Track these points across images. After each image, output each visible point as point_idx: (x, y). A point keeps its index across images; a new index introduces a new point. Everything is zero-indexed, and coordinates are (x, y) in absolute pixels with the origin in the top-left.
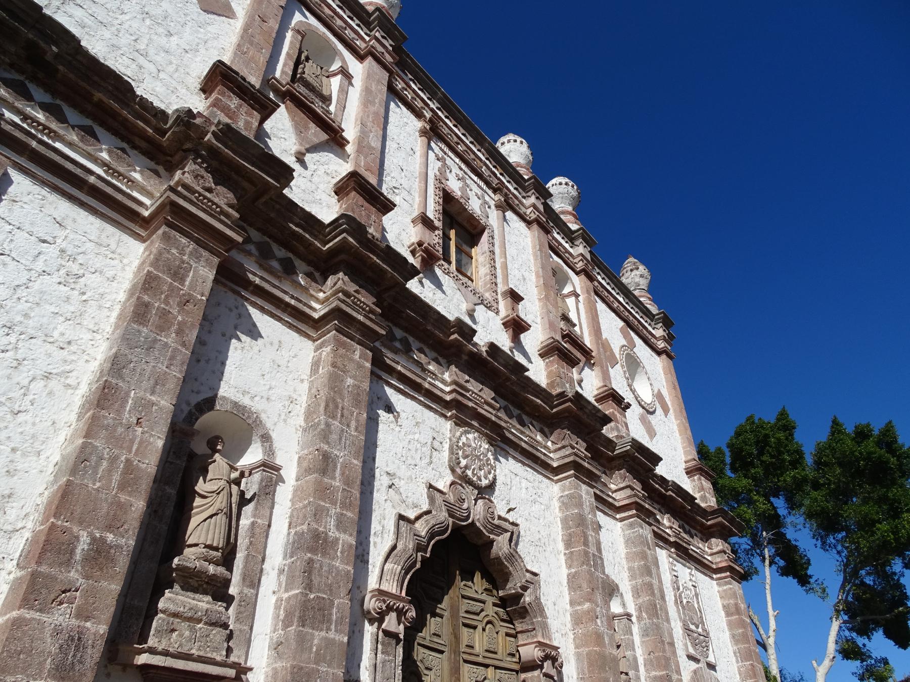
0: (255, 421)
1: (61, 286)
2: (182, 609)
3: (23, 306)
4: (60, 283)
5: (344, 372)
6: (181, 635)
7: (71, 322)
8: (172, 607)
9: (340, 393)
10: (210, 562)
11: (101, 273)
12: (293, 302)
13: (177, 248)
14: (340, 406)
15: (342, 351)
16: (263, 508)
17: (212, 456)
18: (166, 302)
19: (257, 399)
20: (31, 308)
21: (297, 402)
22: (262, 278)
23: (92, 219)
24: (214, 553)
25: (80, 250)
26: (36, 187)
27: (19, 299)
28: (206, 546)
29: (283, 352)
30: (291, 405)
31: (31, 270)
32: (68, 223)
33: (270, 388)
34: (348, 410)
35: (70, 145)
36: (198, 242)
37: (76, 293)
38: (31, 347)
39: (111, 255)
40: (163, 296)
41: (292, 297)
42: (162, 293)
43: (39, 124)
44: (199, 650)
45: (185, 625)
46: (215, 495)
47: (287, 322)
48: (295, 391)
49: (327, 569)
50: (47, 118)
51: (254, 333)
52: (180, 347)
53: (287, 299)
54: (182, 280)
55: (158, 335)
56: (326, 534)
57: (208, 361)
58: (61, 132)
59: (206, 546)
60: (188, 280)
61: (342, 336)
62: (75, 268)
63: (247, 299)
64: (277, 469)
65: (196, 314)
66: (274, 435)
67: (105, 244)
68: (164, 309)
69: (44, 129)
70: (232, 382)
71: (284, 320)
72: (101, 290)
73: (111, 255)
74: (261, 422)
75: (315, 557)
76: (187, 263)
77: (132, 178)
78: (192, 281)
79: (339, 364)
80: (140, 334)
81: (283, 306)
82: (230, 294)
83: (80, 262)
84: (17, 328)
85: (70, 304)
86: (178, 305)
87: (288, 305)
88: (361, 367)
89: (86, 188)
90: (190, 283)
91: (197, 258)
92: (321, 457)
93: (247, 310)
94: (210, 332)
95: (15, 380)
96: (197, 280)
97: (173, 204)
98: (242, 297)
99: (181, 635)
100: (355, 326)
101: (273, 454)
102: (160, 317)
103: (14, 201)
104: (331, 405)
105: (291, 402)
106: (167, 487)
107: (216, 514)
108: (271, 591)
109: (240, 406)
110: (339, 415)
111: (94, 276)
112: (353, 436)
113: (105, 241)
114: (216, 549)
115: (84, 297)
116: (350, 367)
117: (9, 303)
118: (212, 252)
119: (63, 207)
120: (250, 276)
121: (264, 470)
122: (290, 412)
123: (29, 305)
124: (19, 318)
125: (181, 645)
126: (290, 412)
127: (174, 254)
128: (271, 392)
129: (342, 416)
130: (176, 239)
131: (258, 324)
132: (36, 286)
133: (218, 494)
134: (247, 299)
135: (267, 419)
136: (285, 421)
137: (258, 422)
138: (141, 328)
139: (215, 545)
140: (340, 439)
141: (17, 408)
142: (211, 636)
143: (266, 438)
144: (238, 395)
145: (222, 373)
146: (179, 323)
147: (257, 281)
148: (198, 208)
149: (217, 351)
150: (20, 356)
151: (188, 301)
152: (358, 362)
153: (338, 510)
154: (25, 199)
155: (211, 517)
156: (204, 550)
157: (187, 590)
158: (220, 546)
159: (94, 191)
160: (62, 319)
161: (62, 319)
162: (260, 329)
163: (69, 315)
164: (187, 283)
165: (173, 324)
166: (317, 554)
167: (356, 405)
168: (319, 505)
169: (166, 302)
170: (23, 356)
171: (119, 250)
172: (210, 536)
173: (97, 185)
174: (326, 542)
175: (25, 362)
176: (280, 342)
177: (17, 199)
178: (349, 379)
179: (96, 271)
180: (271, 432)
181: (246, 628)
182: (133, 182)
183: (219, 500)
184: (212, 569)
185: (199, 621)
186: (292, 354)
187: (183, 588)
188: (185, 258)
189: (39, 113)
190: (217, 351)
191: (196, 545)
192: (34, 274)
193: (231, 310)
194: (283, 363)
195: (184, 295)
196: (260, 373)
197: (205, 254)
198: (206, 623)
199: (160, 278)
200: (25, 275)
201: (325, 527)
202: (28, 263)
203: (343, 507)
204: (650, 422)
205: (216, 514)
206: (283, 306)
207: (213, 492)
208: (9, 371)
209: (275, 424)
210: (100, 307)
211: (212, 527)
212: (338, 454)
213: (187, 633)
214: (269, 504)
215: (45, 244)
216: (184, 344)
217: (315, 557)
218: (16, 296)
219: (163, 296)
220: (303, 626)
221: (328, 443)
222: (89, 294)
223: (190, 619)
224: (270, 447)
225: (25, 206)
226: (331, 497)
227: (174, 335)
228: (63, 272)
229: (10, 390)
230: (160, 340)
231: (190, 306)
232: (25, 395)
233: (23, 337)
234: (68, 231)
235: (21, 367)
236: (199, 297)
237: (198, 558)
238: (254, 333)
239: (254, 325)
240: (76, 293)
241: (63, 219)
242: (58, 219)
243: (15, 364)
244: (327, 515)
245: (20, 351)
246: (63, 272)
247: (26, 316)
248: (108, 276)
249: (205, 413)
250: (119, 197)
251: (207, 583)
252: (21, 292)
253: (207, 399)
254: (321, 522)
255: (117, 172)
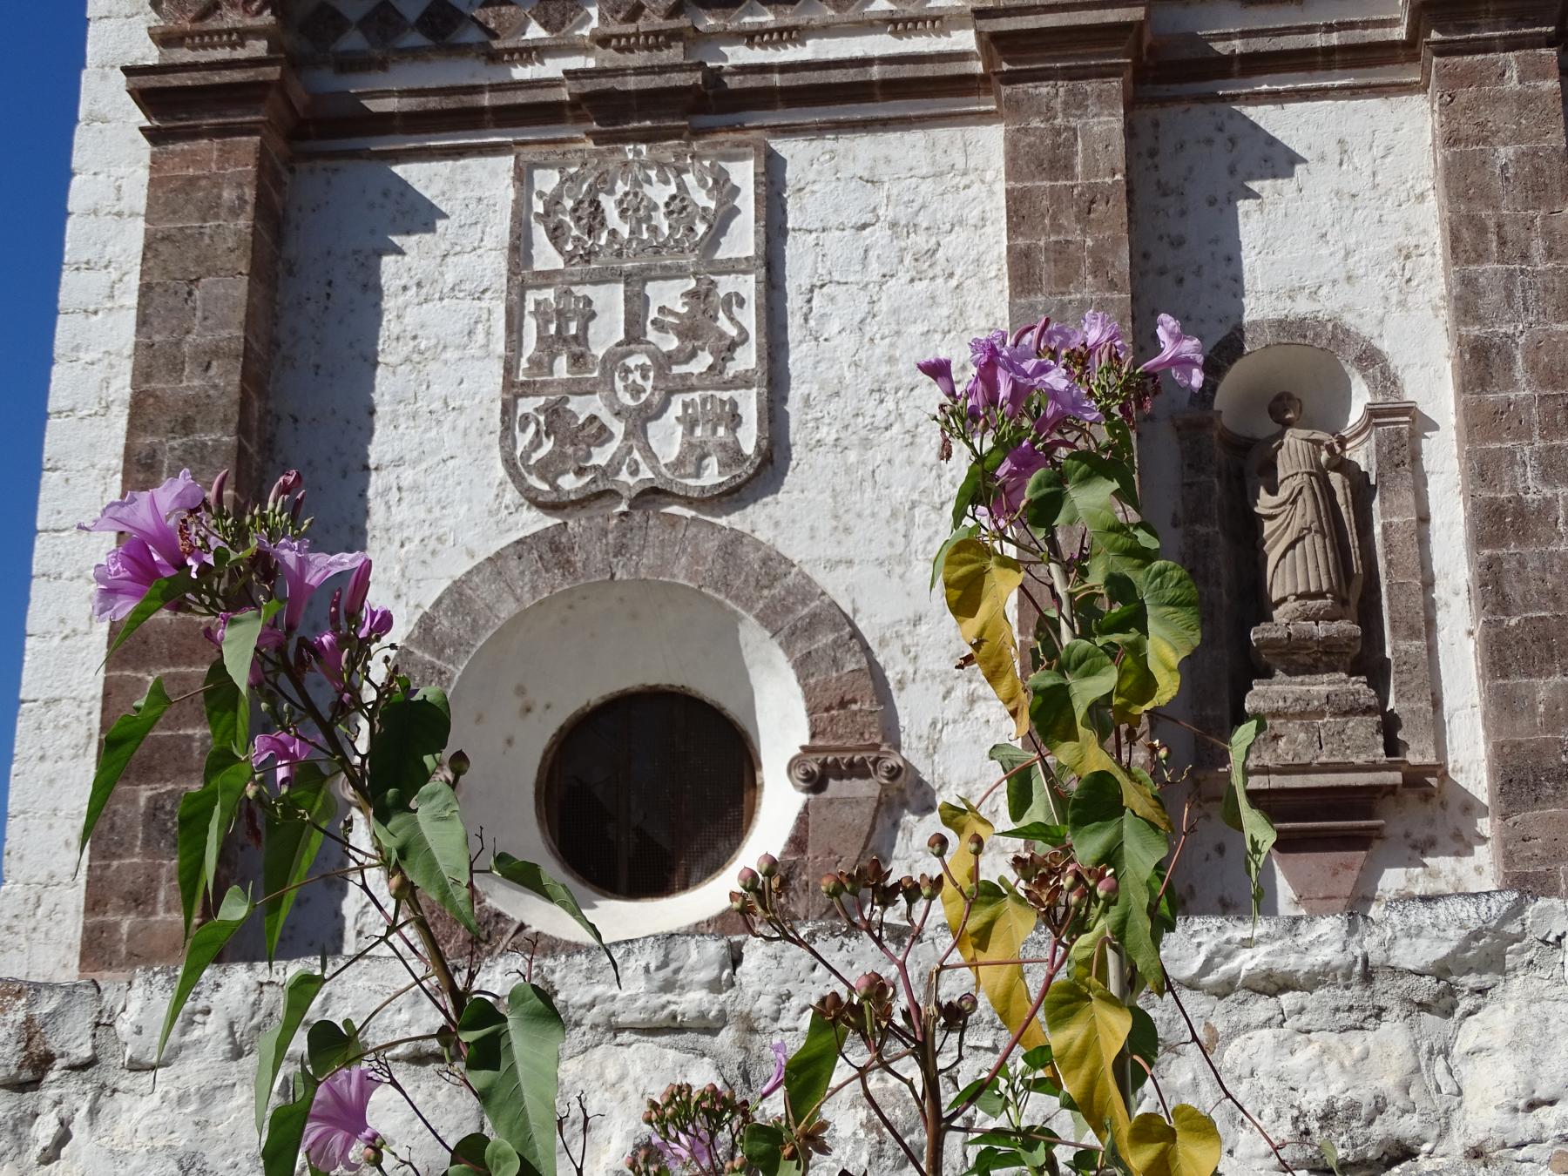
0: (1334, 336)
1: (917, 283)
2: (1281, 704)
3: (882, 347)
4: (912, 281)
5: (1485, 140)
6: (1293, 741)
7: (953, 334)
8: (1263, 706)
9: (1486, 196)
10: (1316, 619)
11: (961, 222)
12: (1335, 39)
13: (1039, 113)
14: (1491, 224)
15: (1465, 94)
16: (1398, 493)
17: (1281, 435)
18: (1057, 228)
19: (1324, 291)
20: (892, 345)
21: (1421, 251)
22: (1245, 34)
23: (916, 137)
24: (1319, 603)
25: (916, 206)
26: (815, 143)
27: (872, 340)
28: (1299, 597)
29: (1356, 160)
30: (1409, 265)
31: (866, 285)
32: (883, 171)
33: (1347, 254)
34: (1515, 222)
35: (827, 30)
36: (1070, 75)
37: (940, 281)
38: (918, 403)
39: (965, 181)
40: (1047, 221)
41: (1329, 28)
42: (1043, 216)
43: (770, 32)
44: (1331, 754)
45: (1295, 725)
46: (1288, 507)
47: (1341, 88)
48: (1408, 229)
49: (1537, 564)
50: (776, 13)
51: (1281, 161)
52: (1107, 295)
53: (1319, 40)
54: (1068, 169)
55: (1063, 294)
56: (1519, 500)
57: (1198, 272)
58: (802, 20)
59: (1299, 597)
60: (1079, 160)
61: (1456, 59)
62: (920, 241)
63: (1234, 98)
64: (1409, 410)
65: (1114, 213)
66: (1385, 346)
67: (946, 168)
68: (1056, 242)
69: (781, 35)
70: (1260, 287)
71: (1333, 89)
72: (973, 254)
73: (965, 181)
74: (1347, 332)
75: (1502, 552)
76: (1067, 129)
77: (935, 13)
78: (1085, 157)
79: (1468, 129)
80: (1036, 310)
81: (1320, 59)
82: (1199, 110)
83: (925, 225)
84: (888, 386)
85: (939, 305)
86: (1078, 220)
87: (1329, 51)
88: (1530, 101)
89: (877, 91)
90: (1084, 165)
91: (1078, 108)
92: (1467, 356)
93: (1245, 118)
94: (1183, 213)
95: (919, 461)
96: (1094, 151)
97: (996, 37)
98: (1223, 98)
99: (1293, 741)
100: (1487, 12)
101: (1394, 383)
102: (1055, 261)
103: (800, 190)
104: (1466, 235)
105: (1407, 257)
106: (1197, 527)
107: (1300, 539)
108: (1462, 633)
109: (1292, 323)
110: (1494, 246)
111: (953, 235)
112: (1542, 274)
113: (944, 162)
114: (1320, 595)
115: (953, 282)
116: (1499, 118)
117: (863, 354)
118: (1103, 73)
119: (863, 149)
120: (1220, 47)
121: (1377, 425)
122: (1409, 280)
123: (887, 341)
124: (884, 369)
125: (1296, 755)
126: (1409, 280)
127: (1036, 128)
128: (1351, 261)
129: (1503, 242)
130: (1030, 97)
131: (1278, 135)
132: (883, 306)
133: (1294, 502)
134: (1234, 98)
135: (1359, 321)
136: (1402, 304)
137: (1340, 335)
138: (1032, 298)
139: (1313, 589)
140: (1510, 296)
141: (937, 500)
142: (1349, 732)
143: (1370, 358)
144: (1280, 306)
145: (1238, 279)
146: (1092, 252)
147: (1238, 46)
148: (1038, 13)
149: (1211, 242)
150: (909, 425)
151: (1092, 202)
152: (1519, 94)
153: (1539, 444)
154: (811, 176)
155: (1292, 546)
156: (1297, 604)
157: (1297, 674)
158: (1325, 587)
159: (893, 89)
160: (938, 337)
161: (938, 337)
162: (1285, 142)
163: (945, 325)
164: (1079, 169)
165: (1081, 260)
166: (1506, 545)
167: (1536, 198)
168: (1488, 451)
169: (1057, 228)
170: (914, 422)
171: (971, 165)
172: (1300, 578)
173: (888, 76)
174: (1524, 516)
175: (921, 429)
176: (1340, 142)
177: (802, 184)
178: (1502, 150)
179: (953, 225)
180: (1376, 343)
181: (1425, 705)
182: (940, 18)
183: (1299, 511)
184: (1321, 630)
185: (1322, 714)
186: (1377, 151)
187: (1288, 673)
188: (1058, 121)
189: (764, 14)
190: (1211, 242)
191: (1284, 600)
192: (873, 289)
193: (1209, 142)
194: (1361, 183)
195: (1081, 195)
196: (1314, 236)
197: (1090, 86)
198: (1334, 715)
199: (1029, 190)
200: (864, 298)
201: (1512, 489)
202: (858, 277)
203: (1549, 433)
204: (774, 565)
205: (1300, 539)
206: (1320, 59)
207: (1284, 503)
208: (906, 453)
209: (1381, 321)
210: (983, 283)
211: (1299, 562)
212: (1511, 331)
213: (1302, 736)
214: (1409, 481)
215: (868, 230)
216: (1113, 285)
217: (1502, 552)
218: (866, 339)
219: (1047, 221)
220: (1506, 676)
221: (1479, 319)
222: (958, 272)
223: (1302, 715)
224: (1383, 373)
225: (816, 187)
226: (1516, 423)
227: (1090, 278)
228: (908, 259)
229: (919, 479)
230: (1070, 302)
231: (1100, 207)
232: (939, 477)
233: (900, 394)
234: (886, 186)
235: (918, 440)
236: (1109, 180)
237: (1293, 620)
238: (1281, 161)
239: (1272, 141)
240: (940, 281)
241: (872, 169)
242: (866, 175)
243: (908, 439)
244: (1512, 463)
245: (907, 417)
246: (908, 259)
247: (891, 360)
248: (972, 222)
249: (1226, 370)
250: (927, 71)
251: (1326, 653)
252: (871, 328)
253: (1219, 343)
254: (1501, 481)
255: (911, 19)
